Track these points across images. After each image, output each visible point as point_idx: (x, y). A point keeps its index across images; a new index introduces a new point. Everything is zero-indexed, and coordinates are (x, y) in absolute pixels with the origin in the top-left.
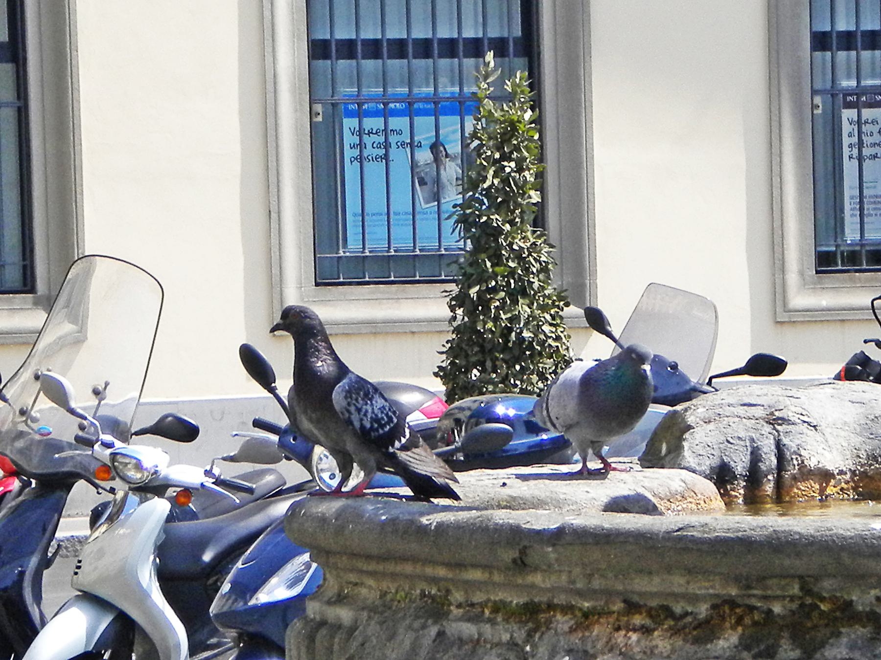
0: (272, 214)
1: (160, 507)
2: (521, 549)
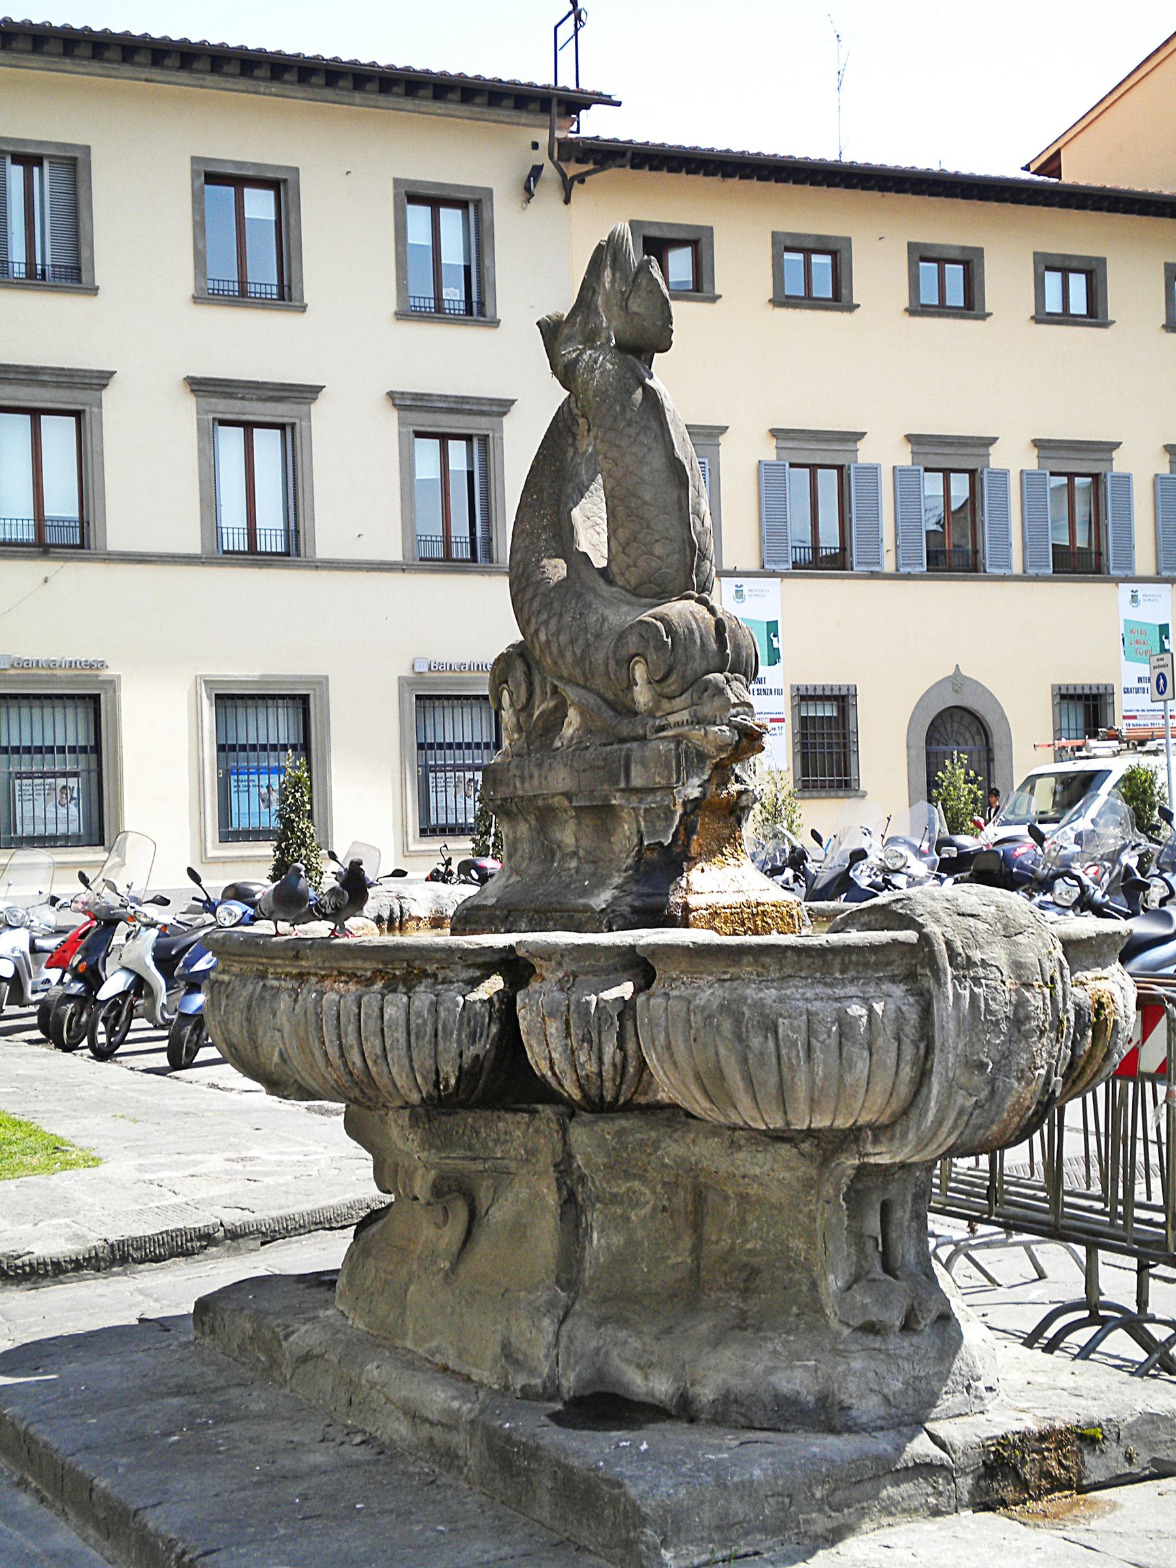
0: (202, 813)
1: (154, 932)
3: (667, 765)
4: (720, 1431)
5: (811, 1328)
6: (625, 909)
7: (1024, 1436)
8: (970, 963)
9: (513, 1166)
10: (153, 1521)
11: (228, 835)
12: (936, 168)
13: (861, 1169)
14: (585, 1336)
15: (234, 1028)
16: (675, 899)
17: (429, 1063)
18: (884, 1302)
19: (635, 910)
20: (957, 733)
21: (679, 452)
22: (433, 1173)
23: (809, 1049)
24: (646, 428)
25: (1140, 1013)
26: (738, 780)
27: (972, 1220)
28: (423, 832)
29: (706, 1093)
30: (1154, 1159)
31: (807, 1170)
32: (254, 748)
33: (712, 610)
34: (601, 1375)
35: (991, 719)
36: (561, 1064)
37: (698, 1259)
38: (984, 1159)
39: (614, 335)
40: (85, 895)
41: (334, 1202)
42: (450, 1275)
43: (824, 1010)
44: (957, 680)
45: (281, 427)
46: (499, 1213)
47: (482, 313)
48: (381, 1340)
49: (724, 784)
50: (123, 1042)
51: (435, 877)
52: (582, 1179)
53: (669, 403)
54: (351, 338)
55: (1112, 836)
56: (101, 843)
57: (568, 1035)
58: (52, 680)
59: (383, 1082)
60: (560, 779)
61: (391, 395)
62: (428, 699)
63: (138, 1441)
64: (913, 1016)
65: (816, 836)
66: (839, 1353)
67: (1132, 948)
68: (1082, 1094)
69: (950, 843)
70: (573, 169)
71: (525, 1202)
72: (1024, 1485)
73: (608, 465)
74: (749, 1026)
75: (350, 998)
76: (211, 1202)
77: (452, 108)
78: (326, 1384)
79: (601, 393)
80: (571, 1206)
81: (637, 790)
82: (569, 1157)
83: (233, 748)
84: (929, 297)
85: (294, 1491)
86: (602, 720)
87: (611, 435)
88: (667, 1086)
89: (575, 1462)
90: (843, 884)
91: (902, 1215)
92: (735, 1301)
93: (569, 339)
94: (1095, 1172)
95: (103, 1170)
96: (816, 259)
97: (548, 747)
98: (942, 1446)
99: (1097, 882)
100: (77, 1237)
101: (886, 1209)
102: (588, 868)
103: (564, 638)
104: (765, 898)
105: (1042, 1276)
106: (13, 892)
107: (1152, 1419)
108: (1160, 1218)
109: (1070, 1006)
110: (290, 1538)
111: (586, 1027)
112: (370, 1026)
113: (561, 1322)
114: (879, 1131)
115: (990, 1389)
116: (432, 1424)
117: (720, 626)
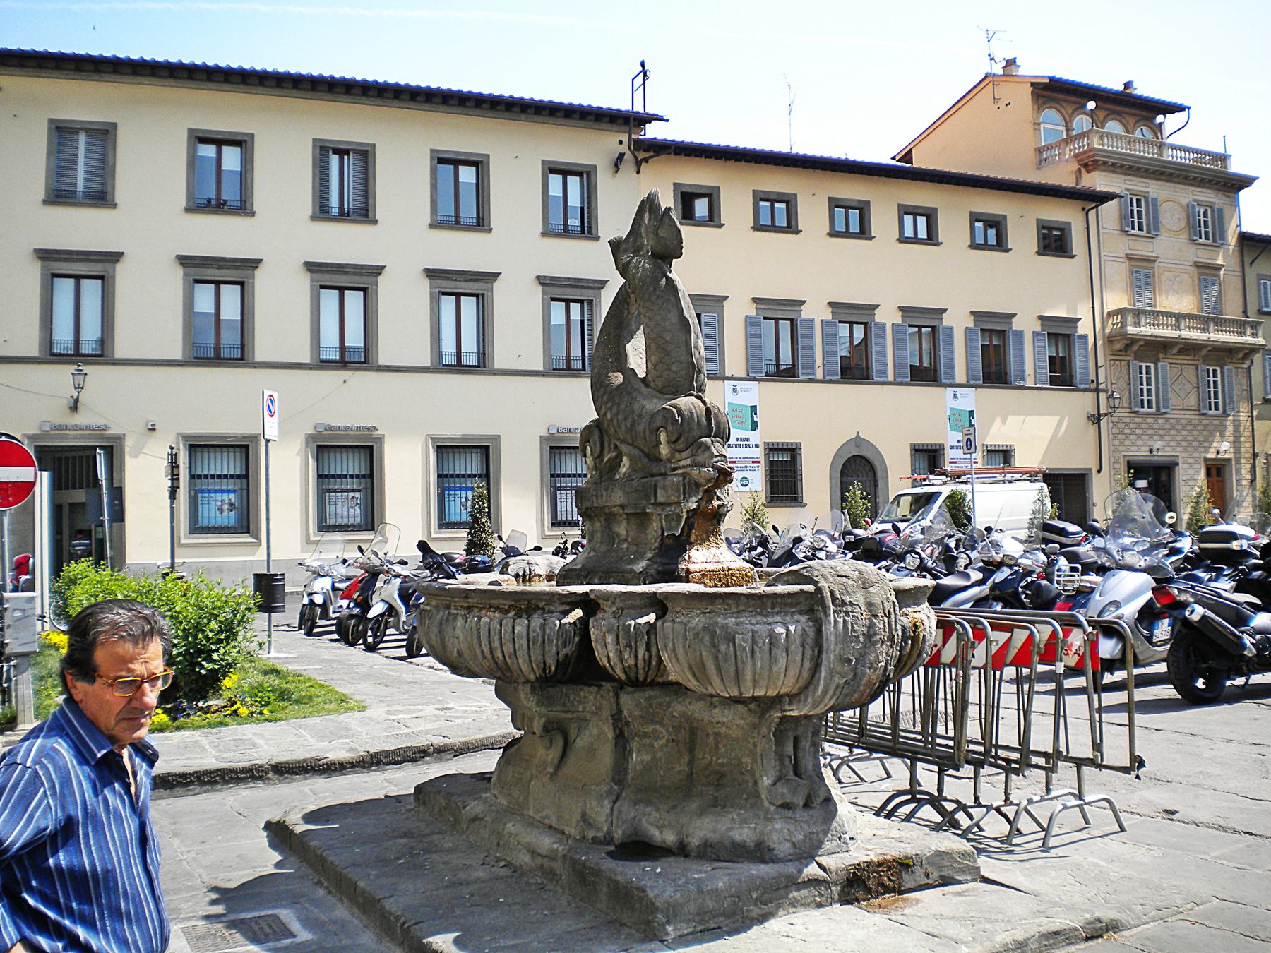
0: (429, 513)
1: (399, 580)
2: (466, 594)
3: (678, 490)
4: (701, 862)
5: (752, 806)
6: (653, 572)
7: (869, 864)
8: (843, 603)
10: (391, 905)
11: (443, 525)
12: (843, 157)
13: (783, 718)
14: (627, 810)
15: (433, 636)
16: (682, 566)
17: (540, 657)
19: (658, 572)
21: (686, 314)
22: (544, 720)
23: (753, 652)
24: (668, 300)
25: (941, 631)
26: (719, 498)
28: (553, 525)
29: (695, 676)
32: (458, 476)
33: (704, 402)
34: (636, 831)
35: (876, 463)
36: (614, 660)
42: (554, 775)
43: (762, 629)
45: (476, 296)
46: (581, 742)
47: (590, 232)
48: (516, 810)
49: (710, 501)
50: (382, 641)
51: (556, 553)
52: (627, 723)
54: (517, 247)
55: (942, 529)
57: (618, 643)
58: (347, 437)
59: (514, 667)
60: (617, 497)
61: (538, 278)
63: (382, 861)
64: (811, 632)
65: (775, 529)
66: (766, 819)
69: (851, 533)
70: (641, 155)
71: (595, 736)
72: (869, 890)
73: (646, 320)
74: (720, 639)
75: (496, 621)
76: (427, 732)
77: (604, 126)
78: (485, 833)
80: (621, 740)
81: (661, 504)
82: (620, 711)
83: (446, 476)
84: (841, 227)
85: (465, 892)
86: (643, 467)
87: (648, 304)
88: (675, 671)
89: (619, 878)
90: (789, 557)
91: (806, 744)
92: (712, 791)
93: (626, 251)
94: (918, 718)
95: (367, 713)
96: (777, 205)
97: (612, 479)
100: (353, 750)
101: (796, 741)
104: (733, 565)
105: (889, 776)
106: (323, 556)
107: (940, 854)
109: (899, 627)
111: (629, 639)
112: (507, 637)
113: (614, 803)
114: (793, 697)
115: (852, 839)
116: (543, 857)
117: (708, 411)
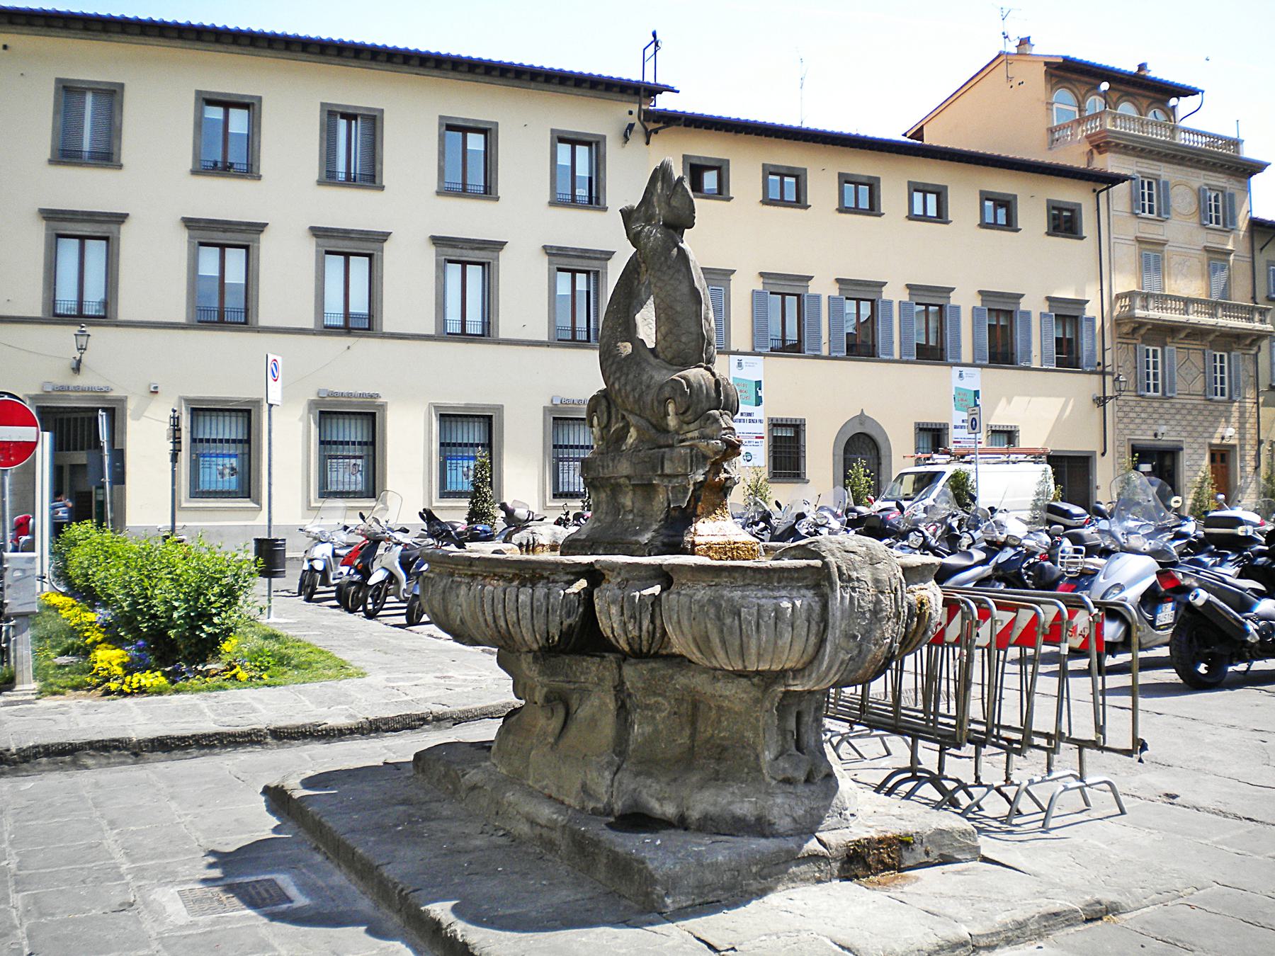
0: (430, 481)
1: (400, 548)
3: (685, 462)
4: (701, 835)
5: (754, 780)
6: (658, 543)
7: (869, 840)
8: (850, 579)
9: (590, 687)
10: (387, 872)
11: (444, 494)
13: (786, 693)
14: (628, 782)
15: (436, 603)
18: (796, 767)
19: (664, 544)
20: (862, 448)
21: (697, 284)
22: (546, 689)
24: (679, 271)
26: (726, 471)
27: (852, 723)
28: (555, 496)
30: (952, 690)
31: (756, 693)
32: (460, 445)
33: (713, 374)
34: (636, 803)
37: (693, 741)
38: (860, 687)
39: (663, 217)
40: (363, 526)
41: (494, 703)
43: (768, 604)
44: (862, 418)
45: (482, 264)
46: (583, 712)
47: (598, 203)
48: (515, 780)
49: (718, 474)
50: (381, 609)
51: (558, 523)
52: (629, 695)
53: (692, 257)
54: (524, 217)
55: (944, 508)
56: (374, 496)
57: (622, 614)
58: (350, 404)
59: (518, 638)
60: (624, 468)
61: (544, 247)
62: (559, 419)
63: (380, 828)
64: (817, 608)
66: (768, 793)
67: (943, 574)
68: (913, 651)
69: (854, 511)
71: (597, 707)
72: (868, 867)
73: (656, 290)
76: (426, 700)
78: (484, 802)
79: (654, 250)
80: (623, 711)
81: (668, 476)
82: (622, 683)
83: (449, 445)
85: (464, 860)
88: (678, 645)
90: (792, 532)
91: (808, 719)
93: (637, 220)
94: (920, 696)
95: (367, 680)
96: (786, 179)
97: (618, 450)
98: (824, 845)
99: (934, 535)
100: (352, 716)
101: (799, 716)
102: (639, 520)
103: (628, 388)
105: (889, 754)
106: (324, 522)
107: (941, 832)
108: (953, 722)
109: (905, 604)
110: (460, 884)
111: (634, 611)
112: (510, 605)
113: (615, 774)
114: (797, 672)
116: (542, 826)
117: (717, 383)
